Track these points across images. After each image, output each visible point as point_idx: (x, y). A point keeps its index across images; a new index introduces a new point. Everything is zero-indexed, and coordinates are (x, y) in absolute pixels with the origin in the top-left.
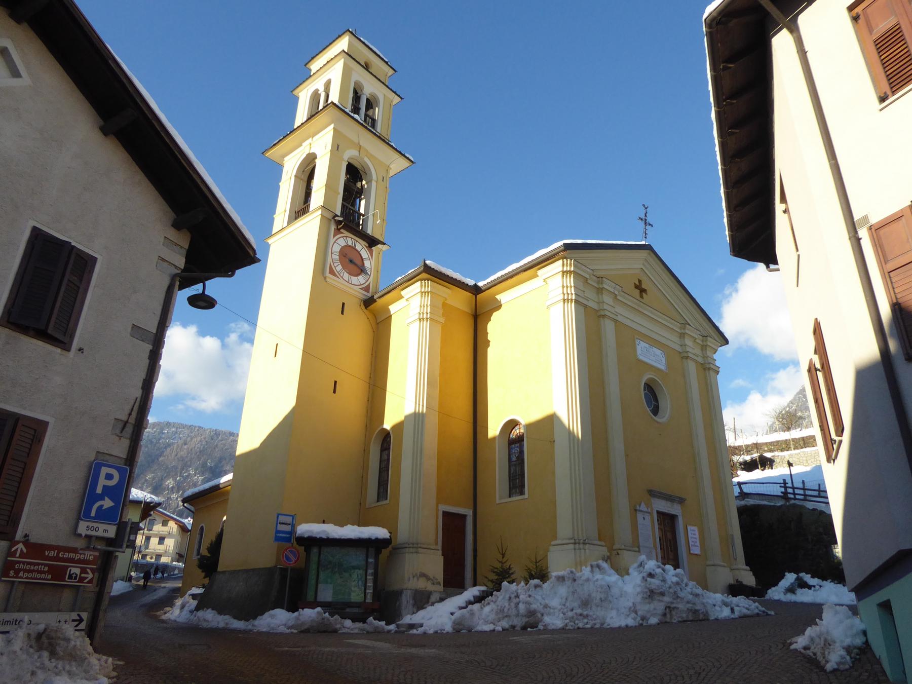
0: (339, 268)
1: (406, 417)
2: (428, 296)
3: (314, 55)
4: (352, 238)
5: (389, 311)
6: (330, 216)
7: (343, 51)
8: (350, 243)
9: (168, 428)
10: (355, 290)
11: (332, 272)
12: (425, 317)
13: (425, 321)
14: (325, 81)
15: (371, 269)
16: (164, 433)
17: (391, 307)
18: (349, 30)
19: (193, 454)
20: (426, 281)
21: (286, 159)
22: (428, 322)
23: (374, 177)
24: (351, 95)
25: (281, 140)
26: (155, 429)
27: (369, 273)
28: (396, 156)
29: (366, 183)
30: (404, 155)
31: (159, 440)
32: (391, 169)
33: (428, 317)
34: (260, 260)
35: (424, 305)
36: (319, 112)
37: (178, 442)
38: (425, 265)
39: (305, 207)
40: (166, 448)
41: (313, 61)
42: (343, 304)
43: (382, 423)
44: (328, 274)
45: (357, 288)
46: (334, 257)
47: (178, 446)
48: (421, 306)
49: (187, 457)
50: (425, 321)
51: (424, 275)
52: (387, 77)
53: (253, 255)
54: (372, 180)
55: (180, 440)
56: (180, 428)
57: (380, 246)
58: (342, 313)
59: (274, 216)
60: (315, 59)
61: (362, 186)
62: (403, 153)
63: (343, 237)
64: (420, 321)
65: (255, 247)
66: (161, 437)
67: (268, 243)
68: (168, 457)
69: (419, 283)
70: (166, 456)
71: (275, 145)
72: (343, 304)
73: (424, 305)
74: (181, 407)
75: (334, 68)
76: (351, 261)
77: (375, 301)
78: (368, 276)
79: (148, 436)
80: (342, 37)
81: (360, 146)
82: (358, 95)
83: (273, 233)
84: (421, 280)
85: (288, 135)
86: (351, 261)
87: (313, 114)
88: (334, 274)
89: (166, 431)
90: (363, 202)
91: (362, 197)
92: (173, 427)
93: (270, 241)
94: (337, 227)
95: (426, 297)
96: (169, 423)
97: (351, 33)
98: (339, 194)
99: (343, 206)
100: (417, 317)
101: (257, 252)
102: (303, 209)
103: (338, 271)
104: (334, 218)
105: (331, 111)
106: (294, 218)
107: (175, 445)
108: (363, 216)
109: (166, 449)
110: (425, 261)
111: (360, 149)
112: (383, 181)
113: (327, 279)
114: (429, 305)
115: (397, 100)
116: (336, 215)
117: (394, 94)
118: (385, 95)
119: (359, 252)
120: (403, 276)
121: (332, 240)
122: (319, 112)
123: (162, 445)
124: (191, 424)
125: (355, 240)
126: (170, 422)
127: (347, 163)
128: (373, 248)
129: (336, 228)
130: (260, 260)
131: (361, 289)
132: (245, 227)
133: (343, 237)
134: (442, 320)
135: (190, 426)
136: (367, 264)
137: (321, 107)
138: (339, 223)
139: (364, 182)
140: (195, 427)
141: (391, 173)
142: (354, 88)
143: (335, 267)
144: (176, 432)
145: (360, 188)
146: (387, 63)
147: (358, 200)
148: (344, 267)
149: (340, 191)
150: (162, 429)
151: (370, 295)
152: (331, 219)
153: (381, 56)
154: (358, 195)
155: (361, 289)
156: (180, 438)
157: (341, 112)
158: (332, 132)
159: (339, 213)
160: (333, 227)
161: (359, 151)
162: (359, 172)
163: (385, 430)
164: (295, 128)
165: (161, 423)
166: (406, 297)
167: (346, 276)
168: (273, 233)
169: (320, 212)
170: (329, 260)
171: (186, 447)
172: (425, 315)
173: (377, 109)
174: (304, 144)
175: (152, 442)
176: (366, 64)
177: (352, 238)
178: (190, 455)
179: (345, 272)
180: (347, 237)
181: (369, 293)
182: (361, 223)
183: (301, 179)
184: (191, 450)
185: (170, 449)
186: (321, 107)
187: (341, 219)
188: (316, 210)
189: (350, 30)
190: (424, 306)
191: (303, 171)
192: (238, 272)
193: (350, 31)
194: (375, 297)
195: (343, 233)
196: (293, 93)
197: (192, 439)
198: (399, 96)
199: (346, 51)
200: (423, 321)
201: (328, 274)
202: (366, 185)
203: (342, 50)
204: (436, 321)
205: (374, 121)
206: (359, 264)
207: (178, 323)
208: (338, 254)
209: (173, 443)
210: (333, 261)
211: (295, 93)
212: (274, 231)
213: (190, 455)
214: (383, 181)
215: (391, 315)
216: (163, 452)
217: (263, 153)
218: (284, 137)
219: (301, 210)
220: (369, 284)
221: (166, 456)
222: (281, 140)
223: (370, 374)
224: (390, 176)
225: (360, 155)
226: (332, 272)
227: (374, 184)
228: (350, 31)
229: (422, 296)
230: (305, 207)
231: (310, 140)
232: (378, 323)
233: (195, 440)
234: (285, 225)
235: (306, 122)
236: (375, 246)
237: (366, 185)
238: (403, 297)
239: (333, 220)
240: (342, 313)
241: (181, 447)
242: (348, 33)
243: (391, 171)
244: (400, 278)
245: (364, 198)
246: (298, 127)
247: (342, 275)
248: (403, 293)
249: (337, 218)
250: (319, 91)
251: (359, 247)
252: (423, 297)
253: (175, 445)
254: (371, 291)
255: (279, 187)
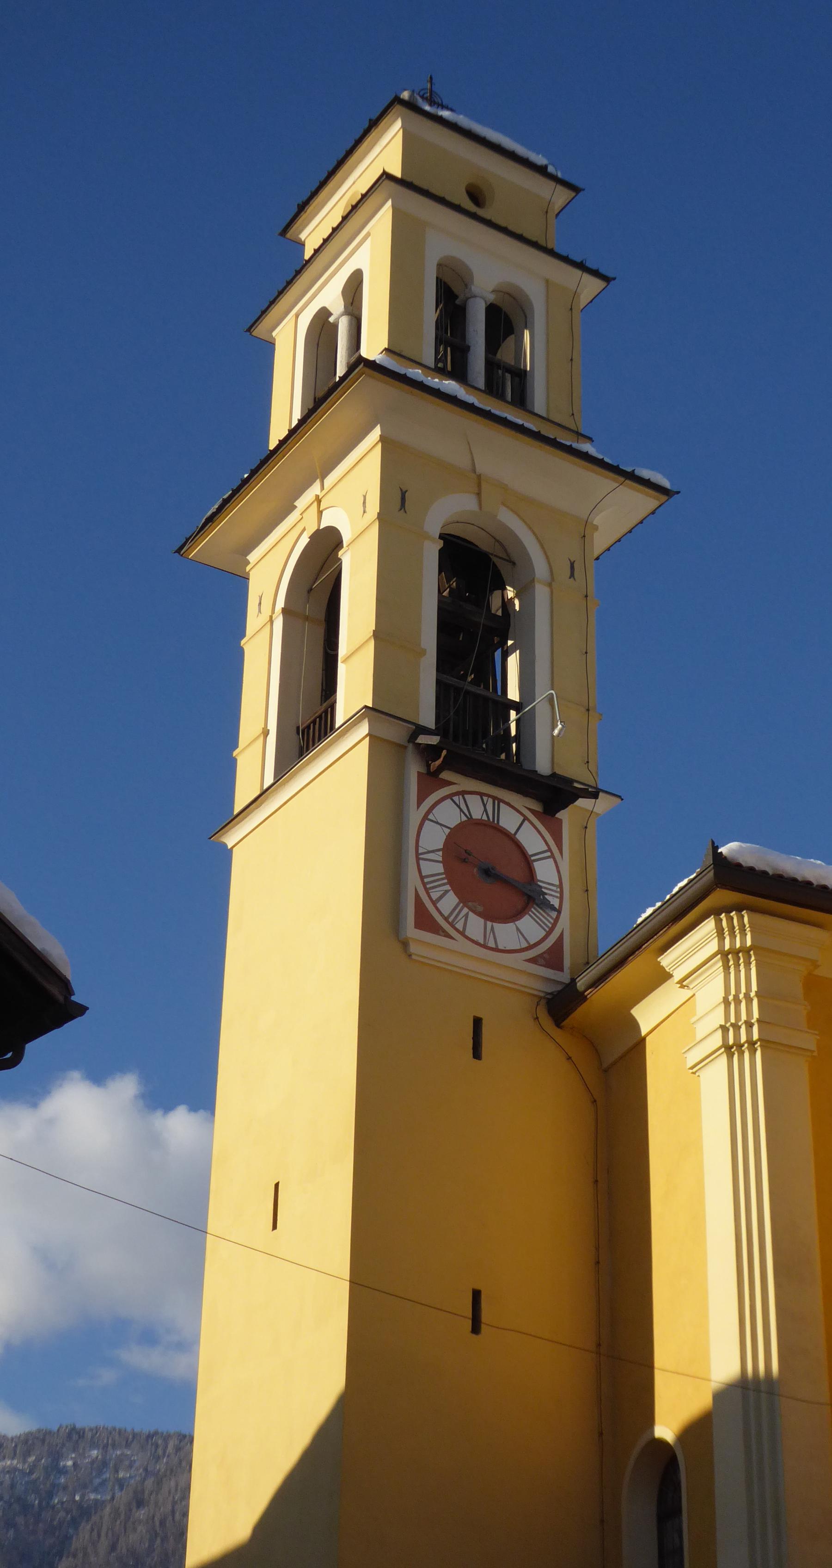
0: (450, 901)
1: (720, 1396)
2: (748, 964)
3: (305, 199)
4: (481, 795)
5: (634, 1025)
6: (396, 733)
7: (386, 176)
8: (477, 813)
9: (74, 1451)
10: (507, 967)
11: (425, 921)
12: (743, 1039)
13: (747, 1055)
14: (314, 313)
15: (561, 886)
16: (63, 1471)
17: (637, 1012)
18: (397, 100)
19: (171, 1540)
20: (733, 914)
21: (252, 557)
22: (758, 1054)
23: (540, 568)
24: (430, 314)
25: (226, 502)
26: (32, 1459)
27: (555, 902)
28: (604, 483)
29: (517, 595)
30: (632, 477)
31: (50, 1495)
32: (596, 528)
33: (756, 1037)
34: (87, 1008)
35: (736, 998)
36: (337, 385)
37: (113, 1498)
38: (719, 861)
39: (326, 712)
40: (75, 1523)
41: (304, 216)
42: (477, 1023)
43: (650, 1420)
44: (411, 931)
45: (518, 961)
46: (428, 868)
47: (116, 1512)
48: (726, 1002)
49: (151, 1550)
50: (747, 1055)
51: (721, 896)
52: (551, 215)
53: (61, 998)
54: (533, 581)
55: (121, 1488)
56: (114, 1446)
57: (581, 802)
58: (477, 1053)
59: (235, 753)
60: (310, 209)
61: (507, 605)
62: (629, 469)
63: (450, 796)
64: (730, 1056)
65: (68, 972)
66: (53, 1485)
67: (225, 845)
68: (86, 1554)
69: (709, 925)
70: (80, 1555)
71: (211, 519)
72: (477, 1023)
73: (736, 997)
74: (107, 1376)
75: (368, 235)
76: (488, 873)
77: (581, 998)
78: (554, 914)
79: (13, 1486)
80: (382, 125)
81: (479, 477)
82: (458, 302)
83: (237, 809)
84: (716, 912)
85: (245, 482)
86: (488, 873)
87: (321, 394)
88: (435, 928)
89: (70, 1463)
90: (513, 662)
91: (510, 643)
92: (93, 1445)
93: (230, 839)
94: (428, 766)
95: (732, 970)
96: (78, 1433)
97: (410, 105)
98: (423, 652)
99: (443, 690)
100: (717, 1040)
101: (75, 985)
102: (320, 717)
103: (446, 914)
104: (413, 737)
105: (365, 382)
106: (296, 750)
107: (108, 1509)
108: (517, 706)
109: (76, 1529)
110: (715, 848)
111: (479, 485)
112: (572, 575)
113: (413, 948)
114: (752, 994)
115: (591, 286)
116: (421, 730)
117: (578, 273)
118: (547, 281)
119: (511, 838)
120: (658, 904)
121: (414, 816)
122: (337, 385)
123: (62, 1514)
124: (152, 1430)
125: (494, 798)
126: (79, 1426)
127: (441, 544)
128: (559, 815)
129: (423, 770)
130: (87, 1008)
131: (533, 960)
132: (33, 919)
133: (450, 796)
134: (809, 1041)
135: (150, 1436)
136: (545, 871)
137: (341, 370)
138: (428, 753)
139: (510, 593)
140: (167, 1438)
141: (600, 542)
142: (439, 281)
143: (434, 903)
144: (104, 1464)
145: (500, 613)
146: (542, 170)
147: (498, 654)
148: (465, 898)
149: (424, 645)
150: (56, 1456)
151: (564, 977)
152: (406, 744)
153: (520, 150)
154: (496, 639)
155: (533, 960)
156: (121, 1483)
157: (397, 383)
158: (376, 455)
159: (428, 718)
160: (414, 769)
161: (479, 494)
162: (490, 559)
163: (662, 1443)
164: (272, 447)
165: (48, 1433)
166: (678, 975)
167: (475, 925)
168: (237, 809)
169: (364, 729)
170: (412, 881)
171: (142, 1514)
172: (743, 1030)
173: (527, 334)
174: (302, 502)
175: (26, 1508)
176: (476, 195)
177: (481, 795)
178: (158, 1541)
179: (471, 914)
180: (463, 793)
181: (561, 969)
182: (513, 732)
183: (307, 618)
184: (162, 1523)
185: (89, 1527)
186: (341, 370)
187: (434, 740)
188: (353, 722)
189: (405, 95)
190: (737, 1001)
191: (310, 590)
192: (32, 1048)
193: (402, 102)
194: (581, 984)
195: (450, 783)
196: (254, 333)
197: (159, 1483)
198: (596, 273)
199: (398, 173)
200: (741, 1054)
201: (411, 931)
202: (517, 602)
203: (381, 171)
204: (790, 1048)
205: (521, 377)
206: (516, 874)
207: (76, 1075)
208: (439, 856)
209: (98, 1505)
210: (424, 884)
211: (260, 331)
212: (239, 804)
213: (158, 1541)
214: (572, 575)
215: (643, 1040)
216: (67, 1538)
217: (178, 551)
218: (236, 492)
219: (314, 722)
220: (561, 938)
221: (80, 1555)
222: (226, 502)
223: (597, 1249)
224: (596, 553)
225: (480, 508)
226: (425, 921)
227: (541, 593)
228: (402, 102)
229: (726, 968)
230: (326, 712)
231: (315, 489)
232: (606, 1071)
233: (173, 1483)
234: (269, 780)
235: (302, 422)
236: (565, 806)
237: (517, 602)
238: (669, 976)
239: (411, 746)
240: (477, 1053)
241: (128, 1518)
242: (398, 108)
243: (596, 535)
244: (650, 911)
245: (513, 649)
246: (282, 443)
247: (459, 926)
248: (666, 960)
249: (423, 739)
250: (330, 314)
251: (509, 820)
252: (732, 970)
253: (108, 1509)
254: (567, 962)
255: (241, 653)
